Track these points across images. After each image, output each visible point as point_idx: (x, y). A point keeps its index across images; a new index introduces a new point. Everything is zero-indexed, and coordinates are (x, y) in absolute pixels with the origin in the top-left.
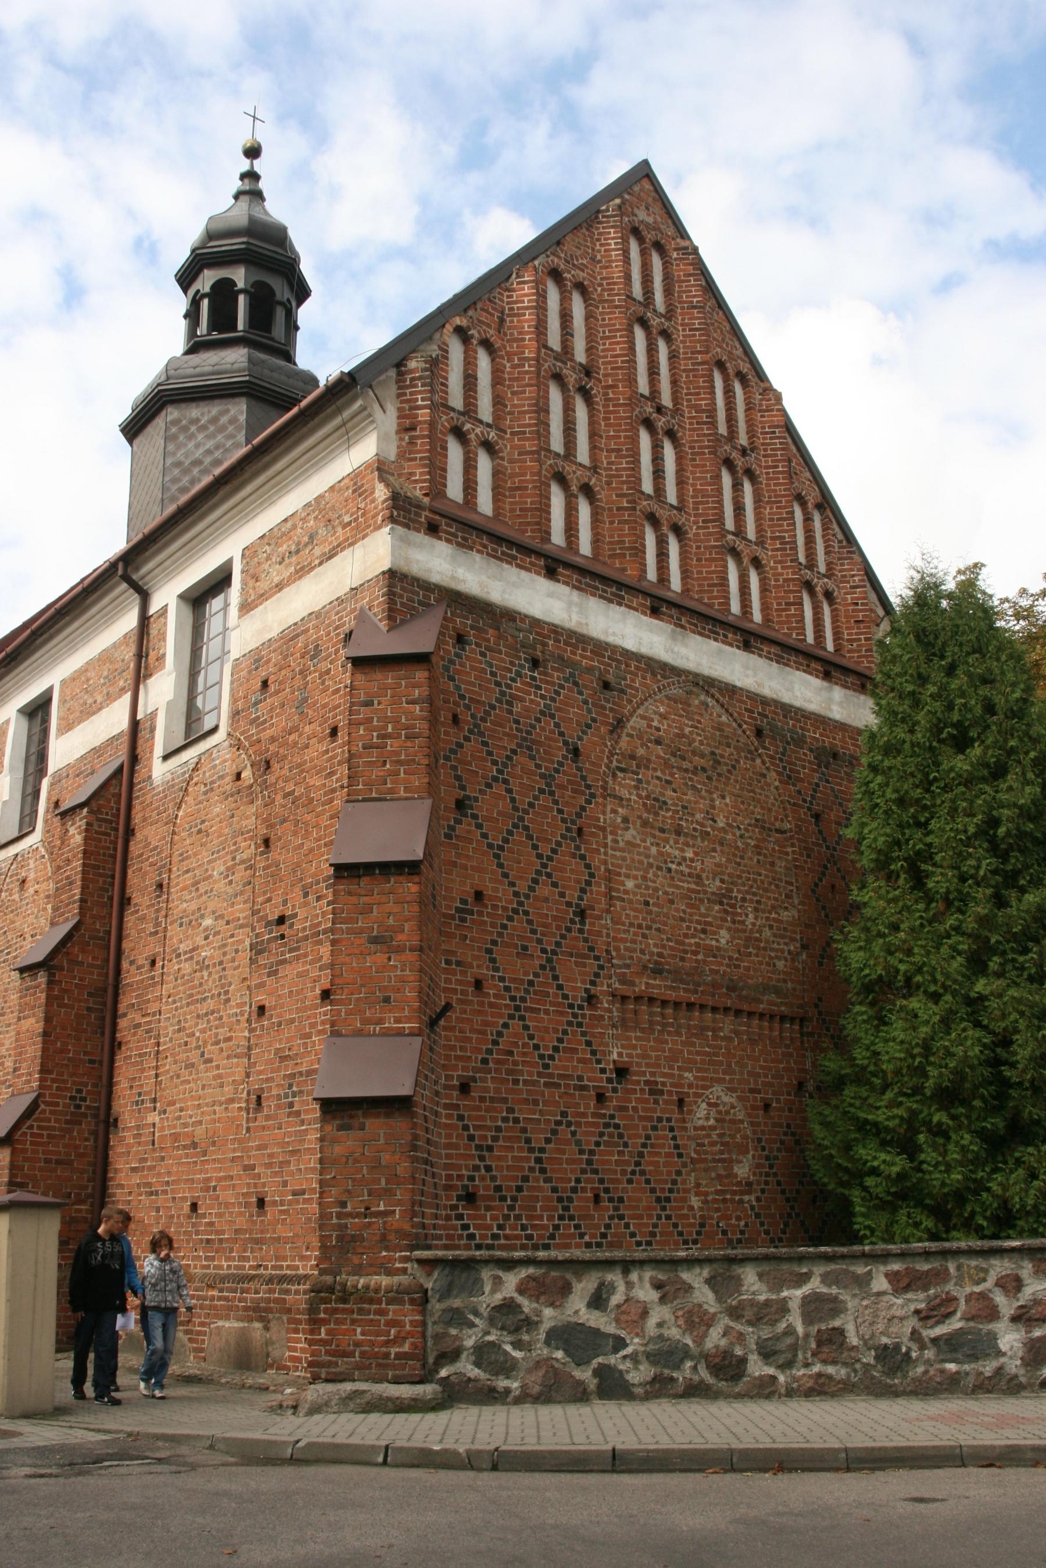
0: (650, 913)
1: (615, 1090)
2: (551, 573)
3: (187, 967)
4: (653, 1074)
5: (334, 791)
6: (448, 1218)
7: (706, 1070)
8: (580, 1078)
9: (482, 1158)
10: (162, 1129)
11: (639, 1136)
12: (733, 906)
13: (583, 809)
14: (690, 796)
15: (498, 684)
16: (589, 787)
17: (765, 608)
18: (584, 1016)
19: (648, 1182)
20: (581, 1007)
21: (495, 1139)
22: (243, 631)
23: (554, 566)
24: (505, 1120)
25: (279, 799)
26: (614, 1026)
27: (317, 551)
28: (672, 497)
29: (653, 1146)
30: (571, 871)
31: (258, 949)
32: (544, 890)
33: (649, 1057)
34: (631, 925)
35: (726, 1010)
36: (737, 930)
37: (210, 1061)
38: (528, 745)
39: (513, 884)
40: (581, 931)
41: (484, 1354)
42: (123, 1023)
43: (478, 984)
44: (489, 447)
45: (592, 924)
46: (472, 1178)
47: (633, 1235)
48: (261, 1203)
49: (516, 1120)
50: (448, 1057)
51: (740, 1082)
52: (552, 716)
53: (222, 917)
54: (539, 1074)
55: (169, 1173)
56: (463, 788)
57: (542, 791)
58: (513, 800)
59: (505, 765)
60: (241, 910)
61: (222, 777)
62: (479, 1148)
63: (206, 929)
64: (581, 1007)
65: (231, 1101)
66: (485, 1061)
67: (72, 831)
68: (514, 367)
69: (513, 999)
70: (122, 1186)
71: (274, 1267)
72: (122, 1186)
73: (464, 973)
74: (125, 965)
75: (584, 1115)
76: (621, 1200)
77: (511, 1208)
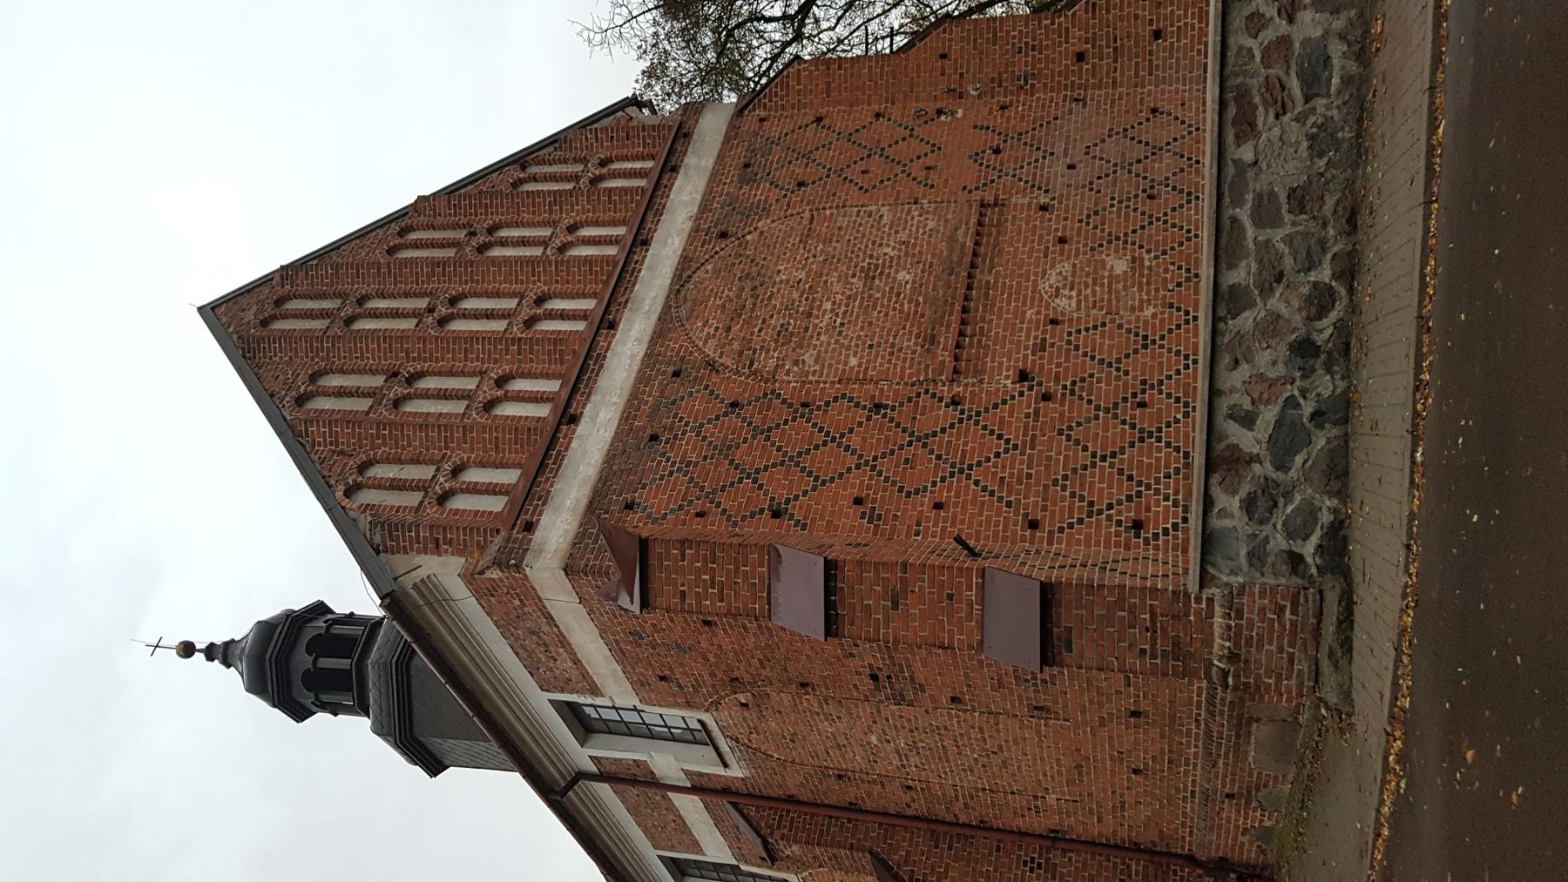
0: (879, 344)
1: (1040, 384)
2: (574, 420)
3: (914, 760)
4: (1026, 348)
5: (760, 627)
6: (1157, 548)
7: (1025, 296)
8: (1028, 416)
9: (1100, 512)
10: (1063, 793)
11: (1084, 362)
12: (877, 266)
13: (784, 401)
14: (776, 302)
15: (671, 474)
16: (765, 395)
17: (613, 223)
18: (970, 410)
19: (1127, 356)
20: (962, 412)
21: (1082, 499)
22: (616, 693)
23: (568, 417)
24: (1064, 488)
25: (766, 673)
26: (981, 382)
27: (546, 628)
28: (511, 304)
29: (1093, 350)
30: (841, 414)
31: (899, 699)
32: (855, 441)
33: (1010, 350)
34: (889, 362)
35: (970, 276)
36: (898, 264)
37: (1000, 747)
38: (726, 450)
39: (849, 469)
40: (893, 409)
41: (1297, 532)
42: (963, 818)
43: (938, 506)
44: (457, 471)
45: (888, 398)
46: (1119, 523)
47: (1178, 372)
48: (1135, 714)
49: (1065, 478)
50: (1005, 539)
51: (1037, 266)
52: (702, 425)
53: (869, 727)
54: (1023, 454)
55: (1105, 790)
56: (762, 510)
57: (768, 438)
58: (774, 465)
59: (743, 471)
60: (865, 710)
61: (745, 719)
62: (1090, 514)
63: (880, 740)
64: (962, 412)
65: (1038, 733)
66: (1009, 504)
67: (788, 852)
68: (385, 444)
69: (952, 475)
70: (1115, 832)
71: (1199, 708)
72: (1115, 832)
73: (928, 519)
74: (910, 812)
75: (1062, 414)
76: (1144, 382)
77: (1148, 487)
